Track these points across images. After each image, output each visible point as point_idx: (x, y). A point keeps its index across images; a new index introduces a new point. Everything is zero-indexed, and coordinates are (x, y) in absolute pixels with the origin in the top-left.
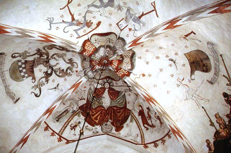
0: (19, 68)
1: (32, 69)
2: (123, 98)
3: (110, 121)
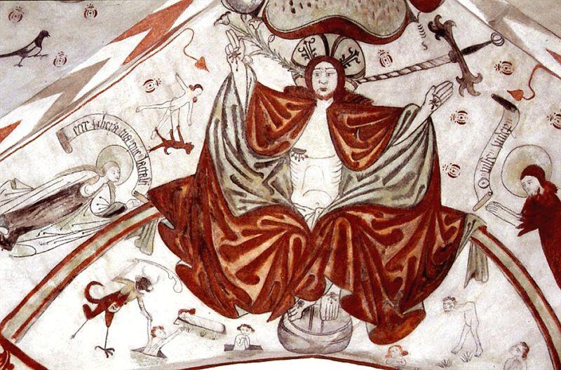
2: (420, 150)
3: (332, 295)
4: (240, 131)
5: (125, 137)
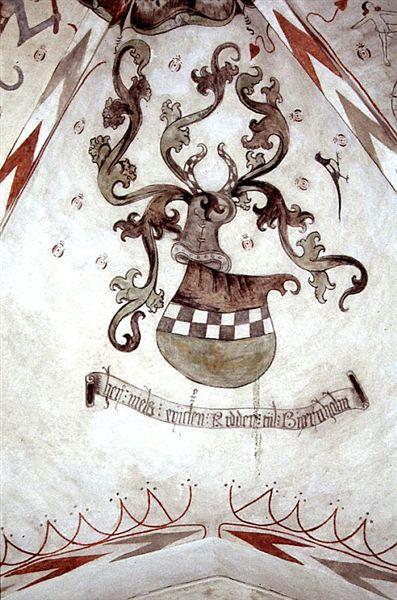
0: (203, 337)
1: (231, 279)
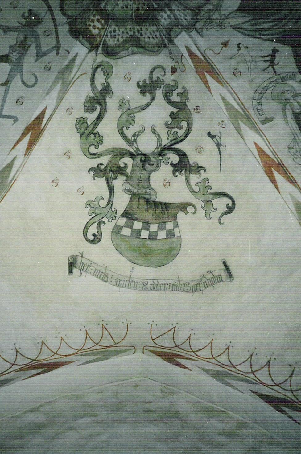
4: (266, 20)
5: (266, 88)
